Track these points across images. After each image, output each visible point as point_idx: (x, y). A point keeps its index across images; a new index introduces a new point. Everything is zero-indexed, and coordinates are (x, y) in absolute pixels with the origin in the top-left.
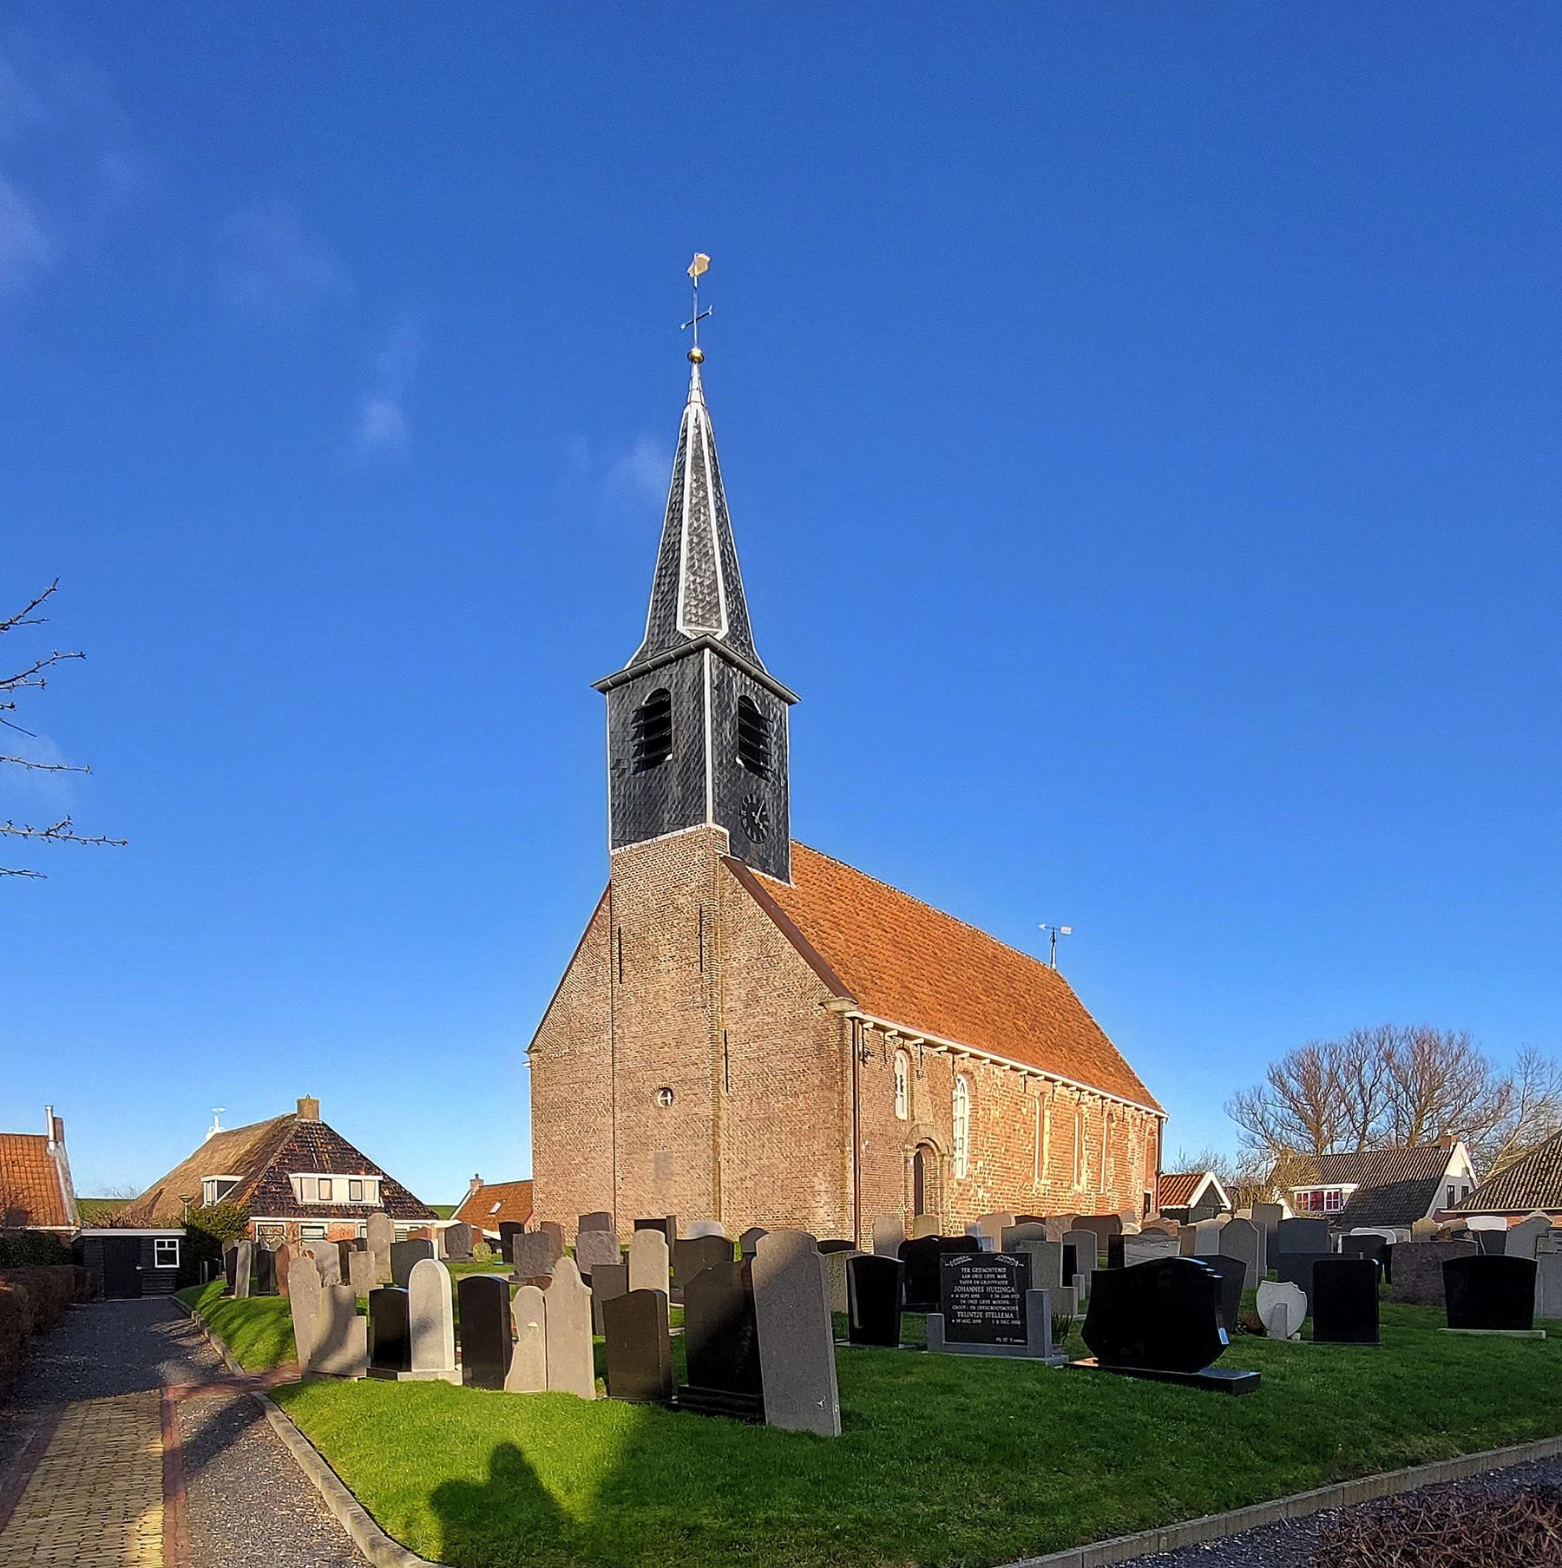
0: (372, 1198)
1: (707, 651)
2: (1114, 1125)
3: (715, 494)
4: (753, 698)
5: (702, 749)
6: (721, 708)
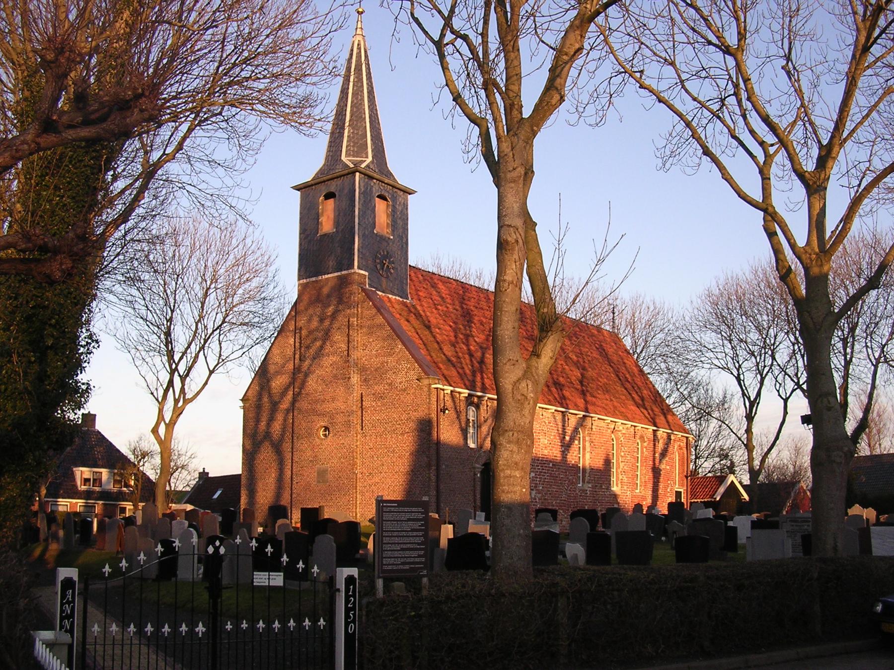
1: (357, 174)
2: (645, 444)
3: (367, 84)
4: (386, 195)
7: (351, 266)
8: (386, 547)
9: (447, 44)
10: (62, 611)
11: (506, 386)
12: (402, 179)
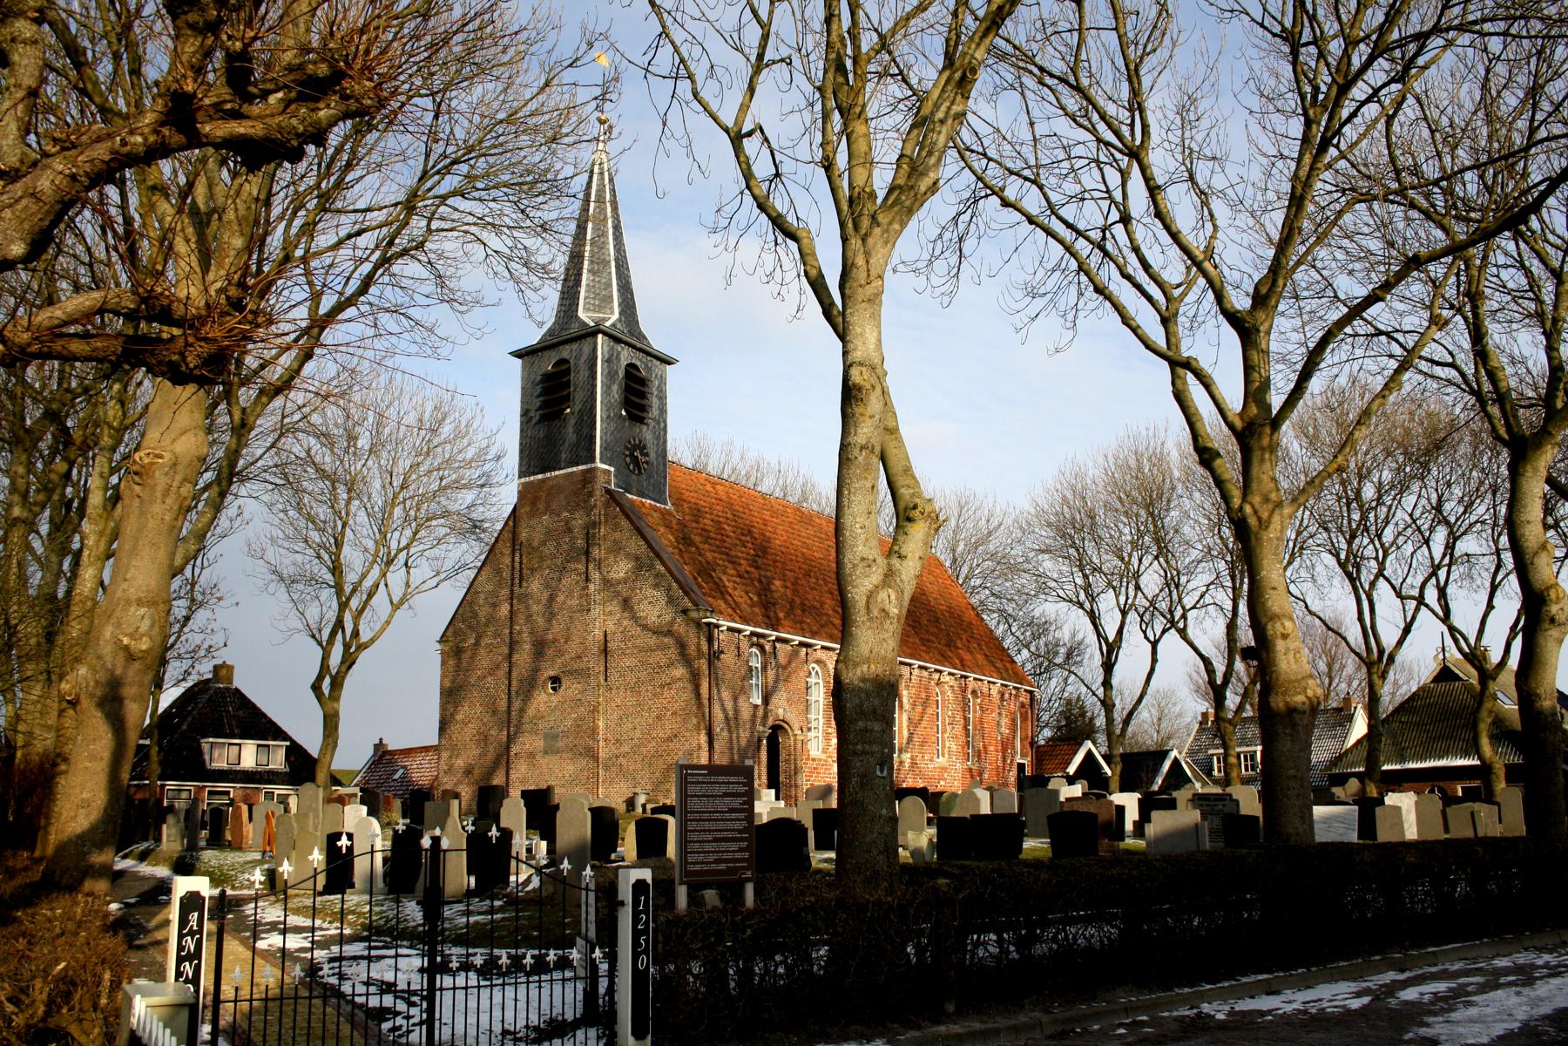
0: (278, 761)
1: (600, 336)
4: (638, 363)
5: (593, 407)
6: (610, 375)
7: (593, 460)
8: (693, 836)
9: (750, 134)
10: (180, 948)
11: (857, 598)
12: (658, 343)
